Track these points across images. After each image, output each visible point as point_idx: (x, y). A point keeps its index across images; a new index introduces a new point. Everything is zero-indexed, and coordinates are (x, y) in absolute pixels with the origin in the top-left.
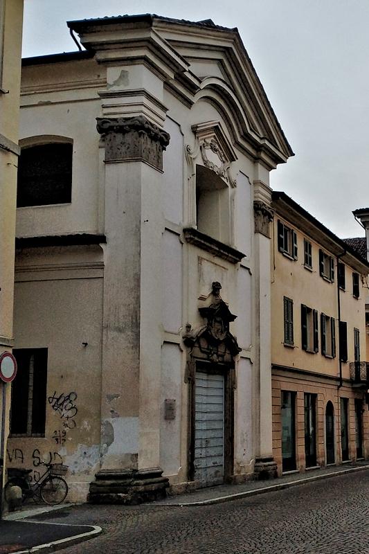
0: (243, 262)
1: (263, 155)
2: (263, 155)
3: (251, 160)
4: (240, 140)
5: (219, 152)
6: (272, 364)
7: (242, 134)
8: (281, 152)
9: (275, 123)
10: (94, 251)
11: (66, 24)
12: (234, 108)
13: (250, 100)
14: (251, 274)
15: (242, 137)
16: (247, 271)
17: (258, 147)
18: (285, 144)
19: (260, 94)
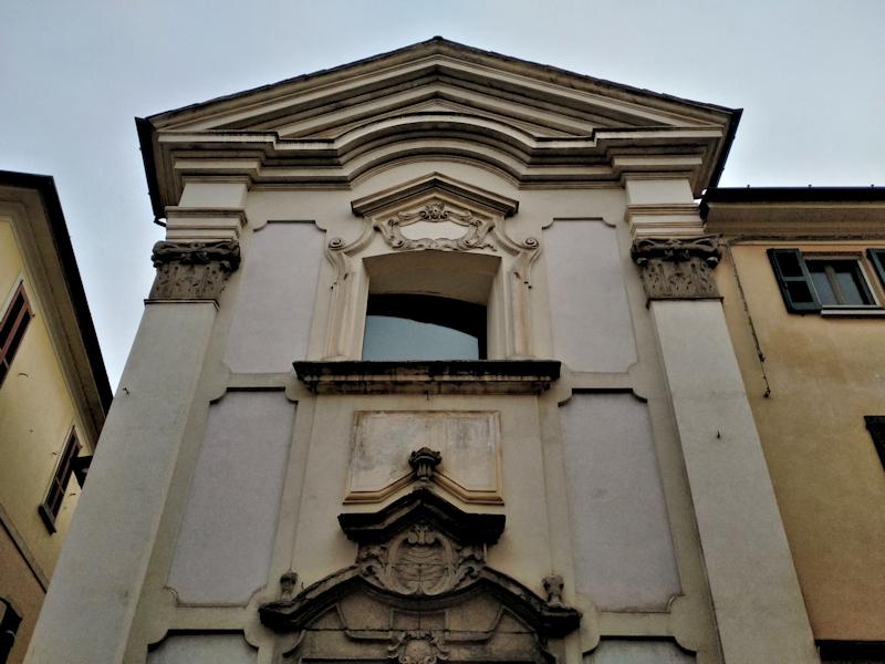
0: (567, 382)
1: (619, 162)
2: (619, 162)
3: (611, 188)
4: (524, 171)
5: (457, 216)
6: (818, 643)
7: (528, 159)
8: (679, 129)
9: (629, 96)
10: (457, 605)
11: (862, 423)
12: (551, 156)
13: (539, 104)
14: (643, 401)
15: (531, 165)
16: (626, 398)
17: (600, 157)
18: (688, 110)
19: (552, 81)
